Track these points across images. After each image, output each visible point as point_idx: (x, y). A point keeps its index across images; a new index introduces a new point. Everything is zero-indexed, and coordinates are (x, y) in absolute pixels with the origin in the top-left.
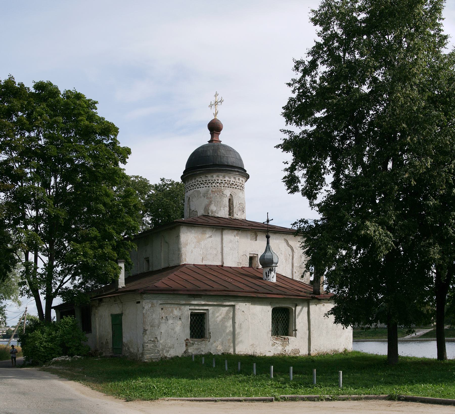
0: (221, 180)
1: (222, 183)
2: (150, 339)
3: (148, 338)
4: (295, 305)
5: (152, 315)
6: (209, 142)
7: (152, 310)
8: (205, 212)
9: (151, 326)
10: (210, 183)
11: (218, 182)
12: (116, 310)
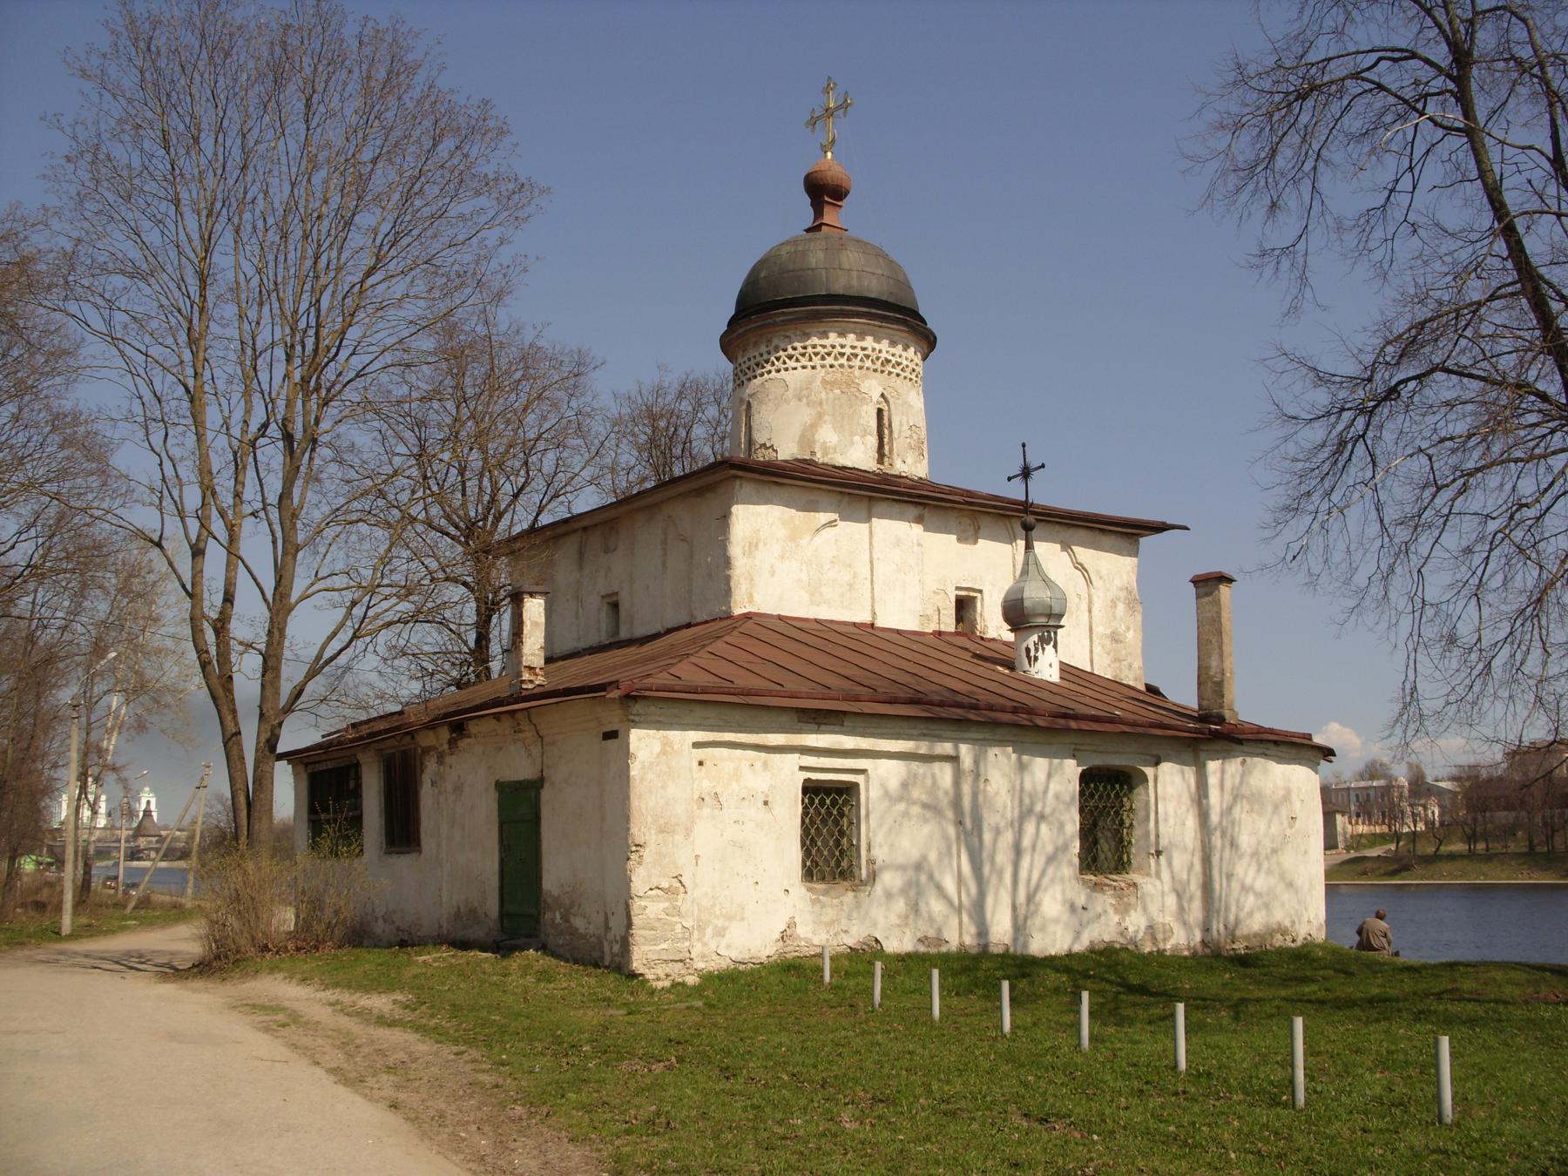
0: (853, 347)
1: (856, 356)
2: (655, 882)
3: (650, 876)
4: (1153, 760)
5: (663, 787)
6: (808, 231)
7: (664, 768)
8: (801, 448)
9: (661, 831)
10: (816, 354)
11: (843, 355)
12: (519, 768)
